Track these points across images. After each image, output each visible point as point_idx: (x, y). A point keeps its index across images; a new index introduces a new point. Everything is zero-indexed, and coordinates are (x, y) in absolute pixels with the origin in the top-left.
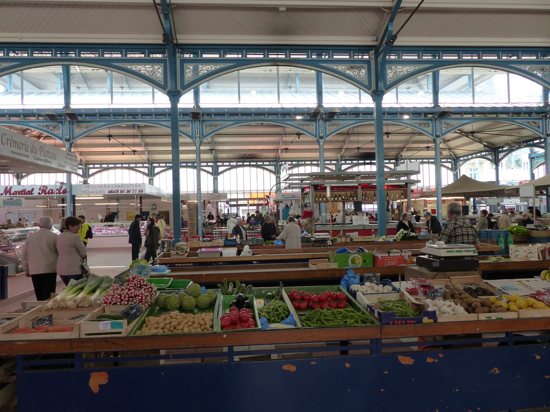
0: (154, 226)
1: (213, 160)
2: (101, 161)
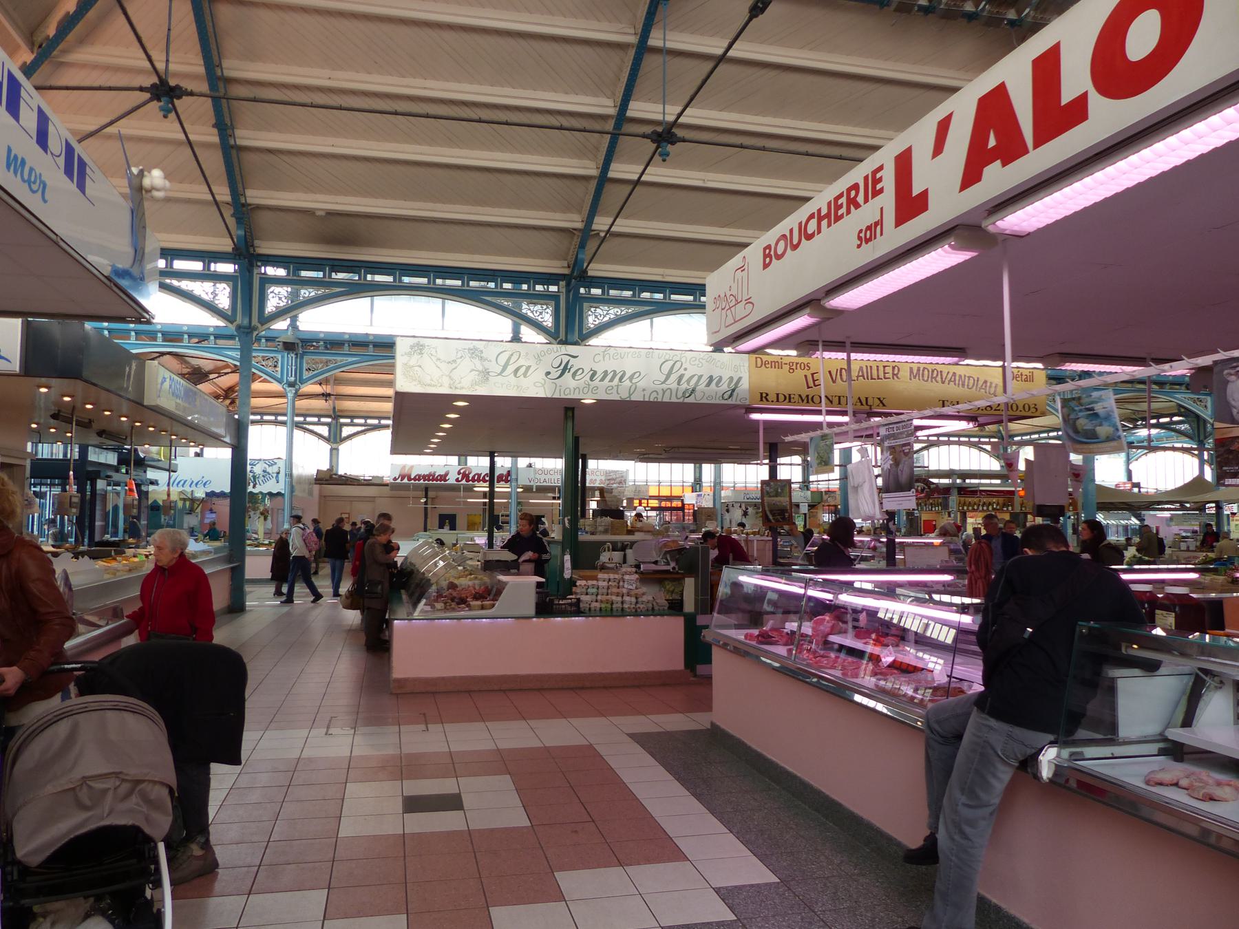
0: (1105, 542)
1: (331, 413)
2: (367, 412)
